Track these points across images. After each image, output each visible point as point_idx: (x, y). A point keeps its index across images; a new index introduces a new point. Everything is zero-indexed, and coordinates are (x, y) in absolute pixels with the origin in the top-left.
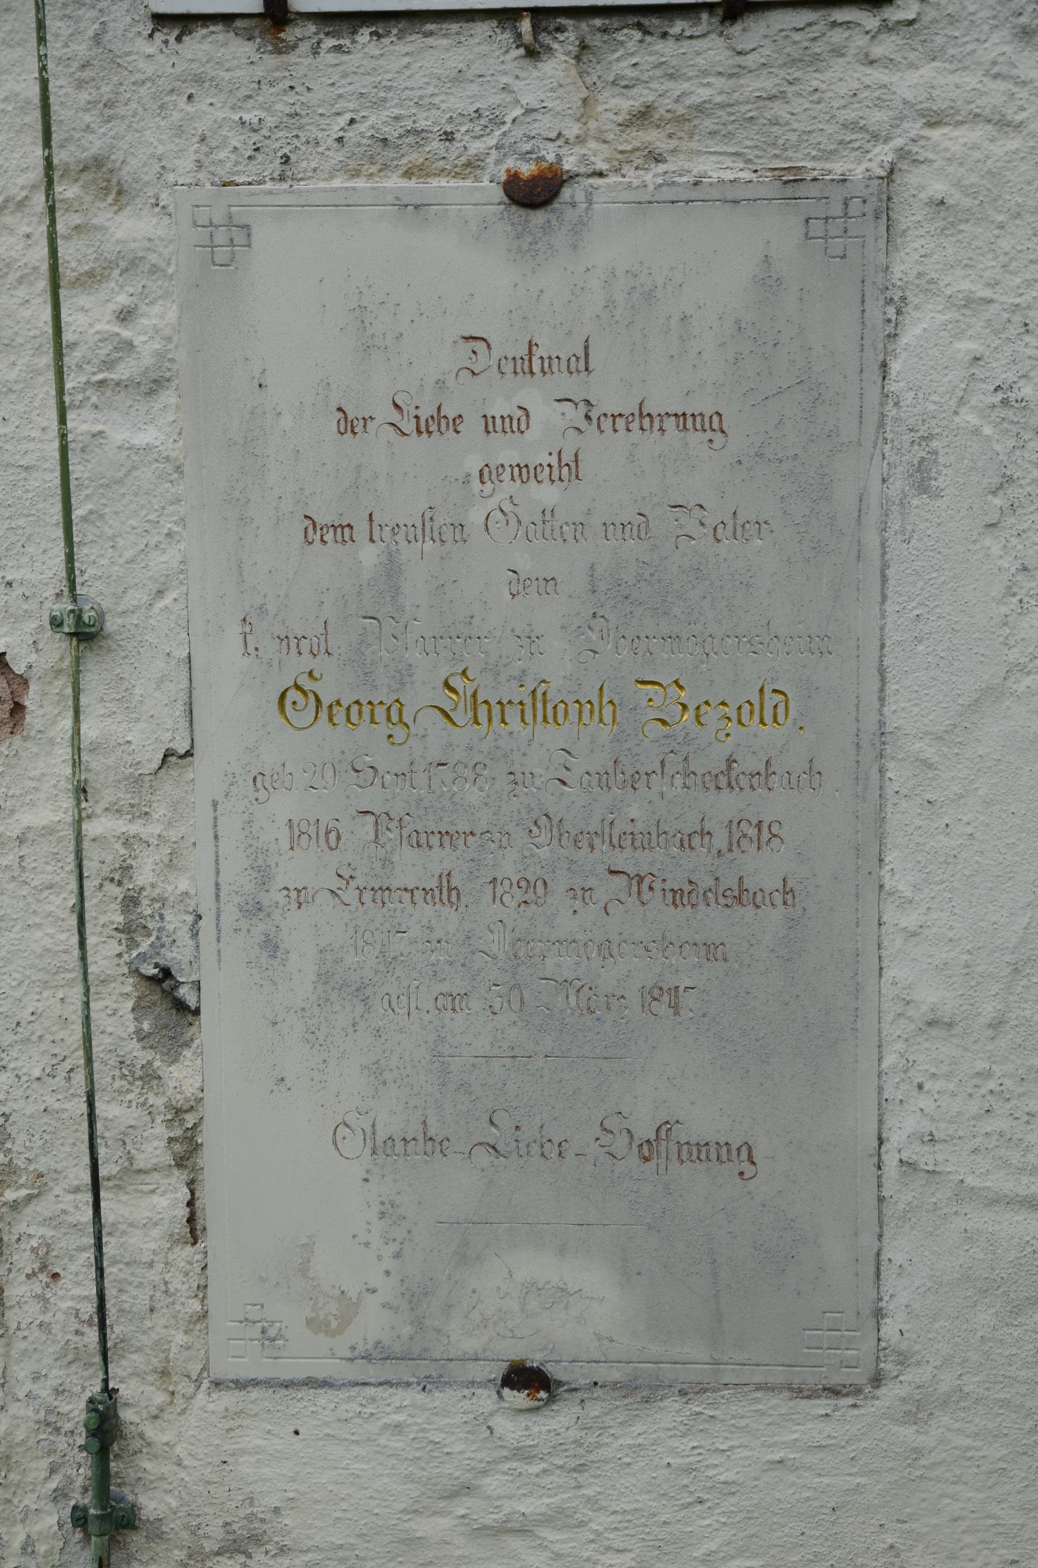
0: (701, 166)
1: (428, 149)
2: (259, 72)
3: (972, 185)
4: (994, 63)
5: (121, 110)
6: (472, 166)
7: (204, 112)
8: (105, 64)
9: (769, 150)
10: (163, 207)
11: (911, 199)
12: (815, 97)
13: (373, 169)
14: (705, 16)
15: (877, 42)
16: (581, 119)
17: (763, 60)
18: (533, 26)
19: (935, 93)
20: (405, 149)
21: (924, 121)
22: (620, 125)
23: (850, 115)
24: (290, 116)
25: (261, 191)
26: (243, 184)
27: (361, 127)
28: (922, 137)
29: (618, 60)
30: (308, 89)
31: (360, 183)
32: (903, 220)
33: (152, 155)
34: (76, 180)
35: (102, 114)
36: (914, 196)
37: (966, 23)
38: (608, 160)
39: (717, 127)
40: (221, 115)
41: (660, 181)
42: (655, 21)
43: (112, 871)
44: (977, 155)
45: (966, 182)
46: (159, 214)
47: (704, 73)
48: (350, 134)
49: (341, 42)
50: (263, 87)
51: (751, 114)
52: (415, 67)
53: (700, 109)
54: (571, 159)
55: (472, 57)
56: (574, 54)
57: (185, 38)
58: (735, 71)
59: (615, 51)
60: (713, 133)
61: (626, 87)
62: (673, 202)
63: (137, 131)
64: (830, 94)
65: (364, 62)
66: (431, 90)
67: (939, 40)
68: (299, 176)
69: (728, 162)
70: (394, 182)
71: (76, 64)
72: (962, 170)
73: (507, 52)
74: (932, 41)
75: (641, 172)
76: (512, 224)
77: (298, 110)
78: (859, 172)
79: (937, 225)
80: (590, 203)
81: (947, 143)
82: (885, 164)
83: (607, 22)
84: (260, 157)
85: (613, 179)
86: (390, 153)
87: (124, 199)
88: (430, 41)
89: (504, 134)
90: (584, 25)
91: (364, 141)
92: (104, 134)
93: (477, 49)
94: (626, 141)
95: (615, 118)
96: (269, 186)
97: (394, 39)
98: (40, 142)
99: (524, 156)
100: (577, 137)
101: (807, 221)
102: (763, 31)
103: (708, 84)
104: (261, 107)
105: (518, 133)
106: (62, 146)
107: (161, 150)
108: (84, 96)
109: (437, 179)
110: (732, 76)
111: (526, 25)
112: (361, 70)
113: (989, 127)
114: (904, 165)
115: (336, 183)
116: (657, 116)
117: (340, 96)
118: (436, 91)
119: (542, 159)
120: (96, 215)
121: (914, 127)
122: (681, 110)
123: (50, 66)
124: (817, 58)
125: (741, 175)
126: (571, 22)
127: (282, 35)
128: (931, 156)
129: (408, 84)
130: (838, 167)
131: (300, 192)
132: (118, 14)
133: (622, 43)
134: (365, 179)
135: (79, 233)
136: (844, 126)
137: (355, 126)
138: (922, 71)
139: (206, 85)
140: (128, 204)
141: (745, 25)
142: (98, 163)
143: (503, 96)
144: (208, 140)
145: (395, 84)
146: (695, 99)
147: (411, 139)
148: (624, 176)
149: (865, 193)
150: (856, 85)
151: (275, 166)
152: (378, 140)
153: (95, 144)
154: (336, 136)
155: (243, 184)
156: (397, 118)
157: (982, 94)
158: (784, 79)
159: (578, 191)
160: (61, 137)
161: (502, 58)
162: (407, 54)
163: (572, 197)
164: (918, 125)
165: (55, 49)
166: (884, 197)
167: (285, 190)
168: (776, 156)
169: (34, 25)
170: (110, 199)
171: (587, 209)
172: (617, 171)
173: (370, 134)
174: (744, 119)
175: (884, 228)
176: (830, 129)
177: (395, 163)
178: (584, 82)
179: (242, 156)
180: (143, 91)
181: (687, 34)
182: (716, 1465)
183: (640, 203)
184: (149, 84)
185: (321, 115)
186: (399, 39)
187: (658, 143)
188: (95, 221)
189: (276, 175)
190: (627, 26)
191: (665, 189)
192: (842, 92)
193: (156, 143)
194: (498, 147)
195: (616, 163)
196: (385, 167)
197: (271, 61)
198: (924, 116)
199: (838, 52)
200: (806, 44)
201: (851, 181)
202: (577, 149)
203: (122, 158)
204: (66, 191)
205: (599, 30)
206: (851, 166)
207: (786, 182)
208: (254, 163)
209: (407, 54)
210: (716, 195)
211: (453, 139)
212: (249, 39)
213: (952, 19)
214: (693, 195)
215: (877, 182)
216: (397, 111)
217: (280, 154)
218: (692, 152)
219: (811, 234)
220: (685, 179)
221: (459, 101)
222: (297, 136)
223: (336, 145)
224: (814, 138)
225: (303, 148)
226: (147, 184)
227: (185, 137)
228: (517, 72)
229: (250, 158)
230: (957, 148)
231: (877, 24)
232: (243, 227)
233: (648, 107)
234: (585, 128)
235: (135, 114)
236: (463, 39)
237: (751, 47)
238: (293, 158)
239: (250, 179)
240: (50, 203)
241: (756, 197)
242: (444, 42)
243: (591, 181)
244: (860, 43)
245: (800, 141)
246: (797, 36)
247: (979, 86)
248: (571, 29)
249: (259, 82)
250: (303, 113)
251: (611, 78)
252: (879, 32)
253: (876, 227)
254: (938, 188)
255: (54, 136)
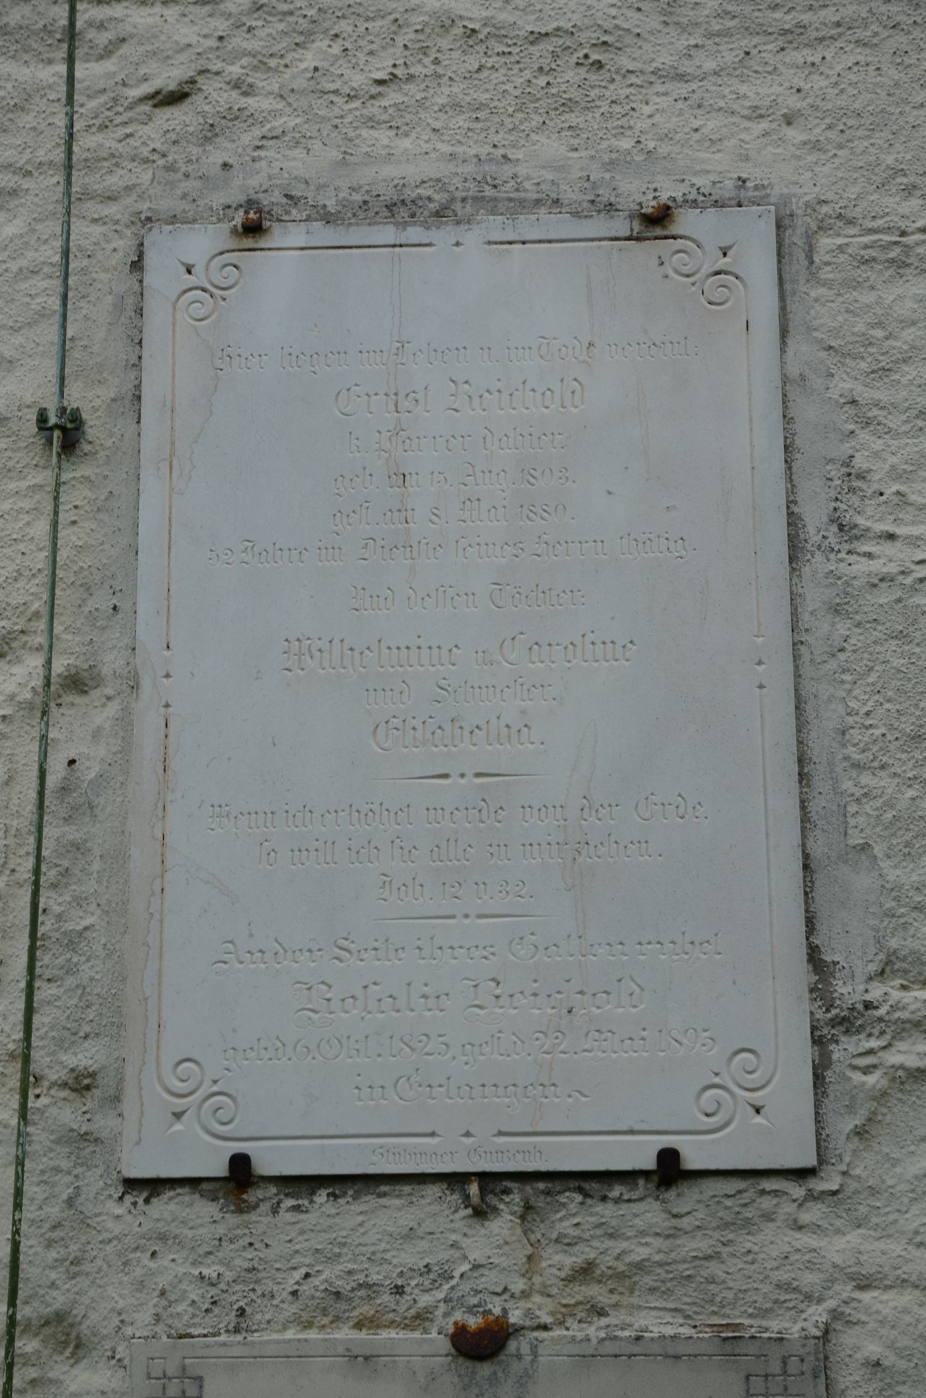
0: (642, 1320)
1: (379, 1302)
2: (221, 1230)
3: (906, 1348)
4: (917, 1233)
5: (87, 1267)
6: (421, 1319)
7: (166, 1268)
8: (75, 1225)
9: (707, 1306)
10: (119, 1360)
11: (847, 1359)
12: (749, 1258)
13: (325, 1321)
14: (641, 1182)
15: (804, 1209)
16: (527, 1274)
17: (697, 1223)
18: (481, 1189)
19: (863, 1258)
20: (357, 1301)
21: (854, 1284)
22: (563, 1280)
23: (784, 1276)
24: (248, 1270)
25: (216, 1343)
26: (199, 1336)
27: (316, 1281)
28: (853, 1299)
29: (561, 1220)
30: (267, 1245)
31: (312, 1334)
32: (841, 1379)
33: (113, 1310)
34: (36, 1335)
35: (67, 1271)
36: (850, 1356)
37: (887, 1195)
38: (552, 1313)
39: (655, 1284)
40: (181, 1270)
41: (602, 1334)
42: (595, 1185)
43: (263, 137)
44: (908, 1318)
45: (899, 1345)
46: (114, 1366)
47: (643, 1233)
48: (305, 1287)
49: (300, 1202)
50: (224, 1244)
51: (688, 1273)
52: (368, 1225)
53: (639, 1266)
54: (517, 1312)
55: (423, 1216)
56: (519, 1214)
57: (154, 1200)
58: (671, 1232)
59: (558, 1211)
60: (652, 1290)
61: (569, 1244)
62: (616, 1356)
63: (100, 1286)
64: (763, 1256)
65: (321, 1221)
66: (383, 1246)
67: (863, 1209)
68: (256, 1327)
69: (668, 1318)
70: (345, 1334)
71: (47, 1226)
72: (895, 1332)
73: (456, 1211)
74: (856, 1210)
75: (584, 1325)
76: (459, 1376)
77: (256, 1265)
78: (795, 1331)
79: (875, 1386)
80: (535, 1354)
81: (879, 1306)
82: (820, 1324)
83: (550, 1185)
84: (216, 1310)
85: (557, 1332)
86: (342, 1306)
87: (81, 1353)
88: (383, 1201)
89: (453, 1288)
90: (528, 1189)
91: (318, 1294)
92: (68, 1290)
93: (427, 1209)
94: (570, 1295)
95: (558, 1273)
96: (223, 1338)
97: (350, 1199)
98: (5, 1299)
99: (471, 1310)
100: (523, 1292)
101: (747, 1378)
102: (696, 1197)
103: (647, 1244)
104: (221, 1262)
105: (466, 1287)
106: (26, 1303)
107: (121, 1303)
108: (53, 1254)
109: (387, 1330)
110: (668, 1237)
111: (474, 1189)
112: (318, 1228)
113: (917, 1293)
114: (838, 1326)
115: (290, 1334)
116: (598, 1272)
117: (297, 1252)
118: (388, 1247)
119: (490, 1312)
120: (52, 1369)
121: (846, 1290)
122: (621, 1267)
123: (24, 1227)
124: (748, 1222)
125: (682, 1330)
126: (517, 1185)
127: (245, 1196)
128: (864, 1318)
129: (361, 1241)
130: (775, 1325)
131: (253, 1344)
132: (92, 1179)
133: (564, 1205)
134: (317, 1331)
135: (34, 1387)
136: (778, 1286)
137: (309, 1280)
138: (848, 1237)
139: (170, 1242)
140: (84, 1357)
141: (680, 1191)
142: (59, 1317)
143: (452, 1252)
144: (168, 1294)
145: (349, 1241)
146: (634, 1258)
147: (362, 1293)
148: (567, 1329)
149: (802, 1352)
150: (787, 1248)
151: (231, 1319)
152: (331, 1293)
153: (58, 1300)
154: (290, 1290)
155: (199, 1336)
156: (350, 1273)
157: (907, 1261)
158: (718, 1240)
159: (523, 1344)
160: (26, 1294)
161: (451, 1217)
162: (361, 1213)
163: (518, 1349)
164: (849, 1288)
165: (29, 1212)
166: (821, 1356)
167: (239, 1343)
168: (714, 1313)
169: (12, 1191)
170: (67, 1353)
171: (533, 1361)
172: (561, 1323)
173: (323, 1287)
174: (682, 1277)
175: (823, 1388)
176: (765, 1288)
177: (347, 1315)
178: (528, 1240)
179: (199, 1308)
180: (109, 1248)
181: (626, 1197)
182: (708, 172)
183: (584, 1356)
184: (115, 1242)
185: (278, 1269)
186: (354, 1199)
187: (600, 1298)
188: (51, 1375)
189: (231, 1327)
190: (569, 1190)
191: (607, 1343)
192: (775, 1254)
193: (117, 1298)
194: (446, 1300)
195: (560, 1316)
196: (337, 1319)
197: (233, 1219)
198: (854, 1280)
199: (768, 1217)
200: (737, 1209)
201: (788, 1340)
202: (523, 1304)
203: (83, 1313)
204: (26, 1345)
205: (543, 1192)
206: (787, 1325)
207: (725, 1339)
208: (211, 1315)
209: (361, 1213)
210: (657, 1349)
211: (403, 1292)
212: (213, 1200)
213: (873, 1191)
214: (636, 1349)
215: (813, 1342)
216: (350, 1266)
217: (235, 1307)
218: (633, 1306)
219: (752, 1391)
220: (626, 1333)
221: (409, 1257)
222: (254, 1290)
223: (290, 1298)
224: (751, 1296)
225: (259, 1301)
226: (105, 1337)
227: (145, 1291)
228: (465, 1230)
229: (207, 1311)
230: (888, 1311)
231: (803, 1193)
232: (195, 1379)
233: (590, 1264)
234: (530, 1283)
235: (100, 1270)
236: (415, 1200)
237: (686, 1210)
238: (249, 1310)
239: (205, 1332)
240: (9, 1360)
241: (697, 1352)
242: (397, 1202)
243: (536, 1334)
244: (788, 1210)
245: (736, 1298)
246: (728, 1202)
247: (904, 1253)
248: (516, 1191)
249: (220, 1239)
250: (261, 1268)
251: (554, 1236)
252: (805, 1200)
253: (815, 1386)
254: (873, 1349)
255: (20, 1292)
